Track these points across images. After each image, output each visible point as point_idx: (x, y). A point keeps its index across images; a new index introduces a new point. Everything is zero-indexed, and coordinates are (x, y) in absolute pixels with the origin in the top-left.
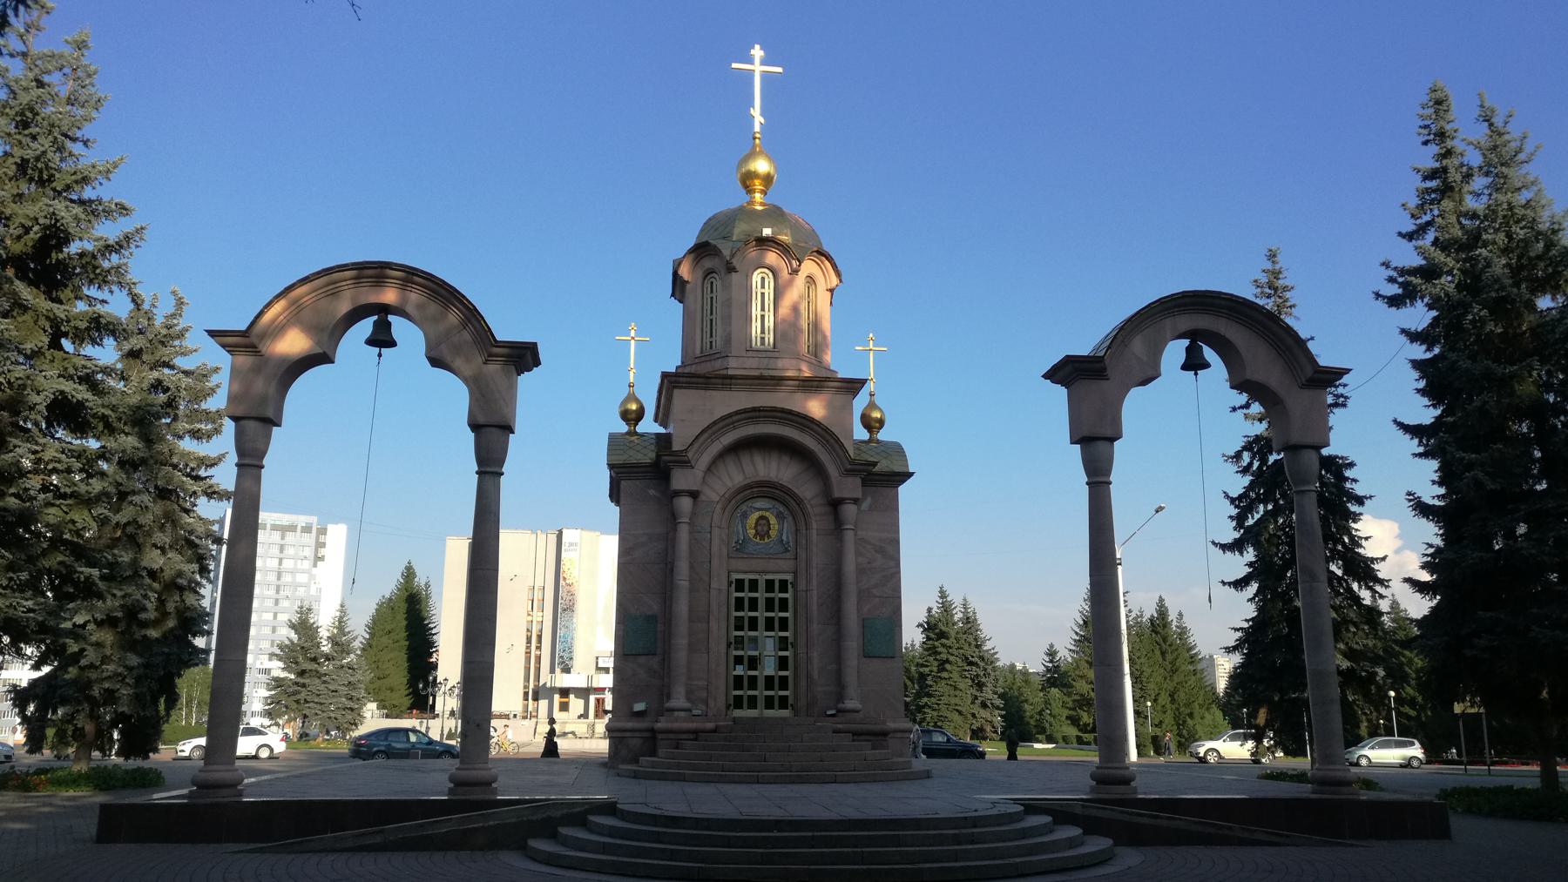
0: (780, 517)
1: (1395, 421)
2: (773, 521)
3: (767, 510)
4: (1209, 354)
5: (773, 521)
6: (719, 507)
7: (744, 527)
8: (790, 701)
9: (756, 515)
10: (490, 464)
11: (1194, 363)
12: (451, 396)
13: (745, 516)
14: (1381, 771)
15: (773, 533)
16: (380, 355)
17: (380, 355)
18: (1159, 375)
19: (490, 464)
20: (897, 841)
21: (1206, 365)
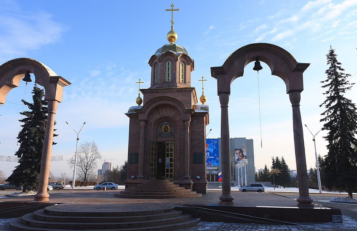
0: (171, 126)
1: (23, 101)
2: (169, 127)
3: (167, 124)
4: (262, 64)
5: (169, 127)
6: (153, 124)
7: (161, 129)
8: (173, 175)
9: (164, 126)
10: (295, 102)
11: (258, 68)
12: (279, 85)
13: (161, 126)
14: (289, 194)
15: (169, 131)
16: (27, 83)
17: (27, 83)
18: (212, 76)
19: (295, 102)
20: (122, 220)
21: (261, 68)
